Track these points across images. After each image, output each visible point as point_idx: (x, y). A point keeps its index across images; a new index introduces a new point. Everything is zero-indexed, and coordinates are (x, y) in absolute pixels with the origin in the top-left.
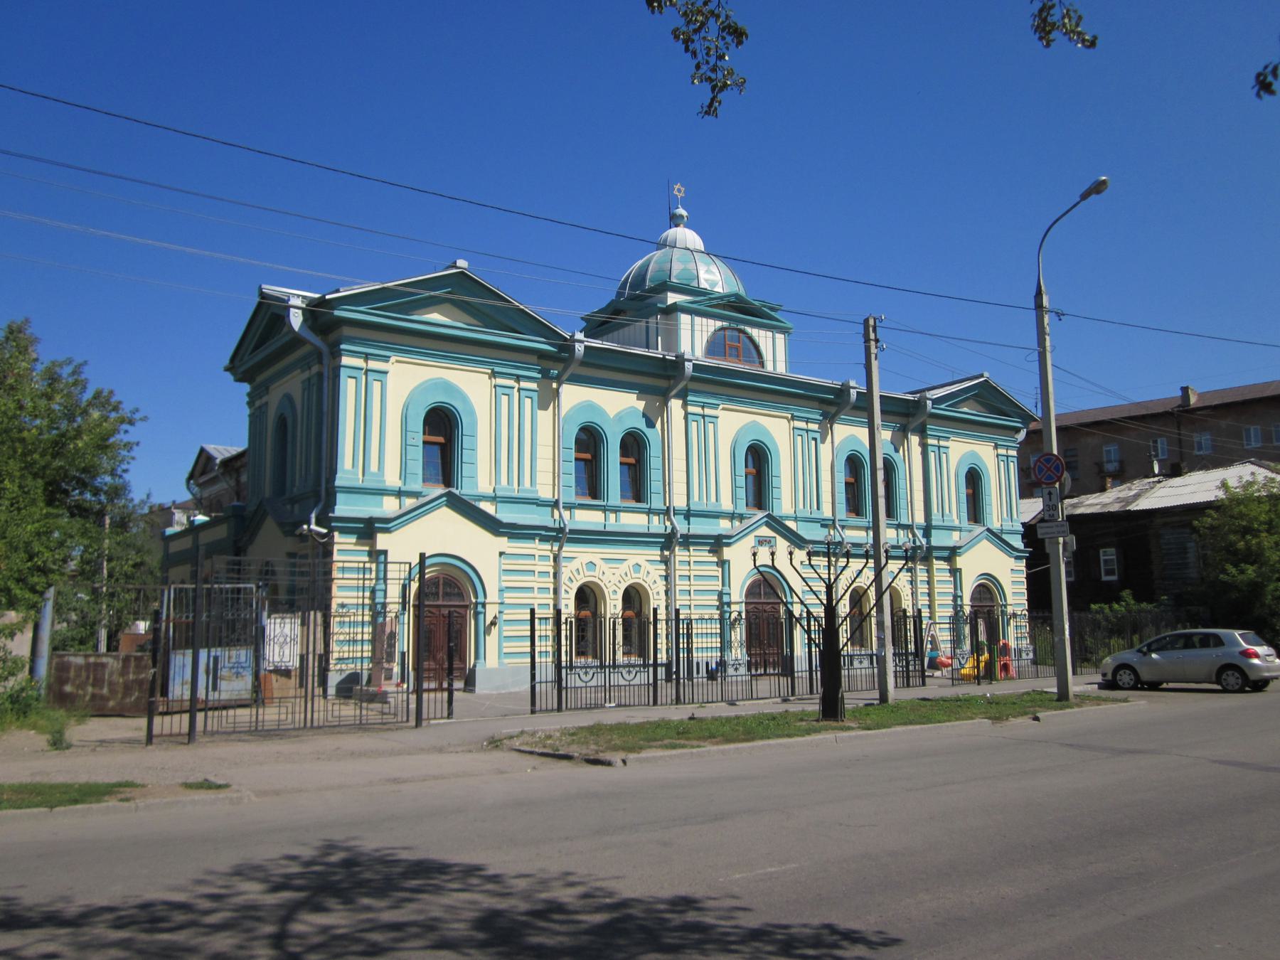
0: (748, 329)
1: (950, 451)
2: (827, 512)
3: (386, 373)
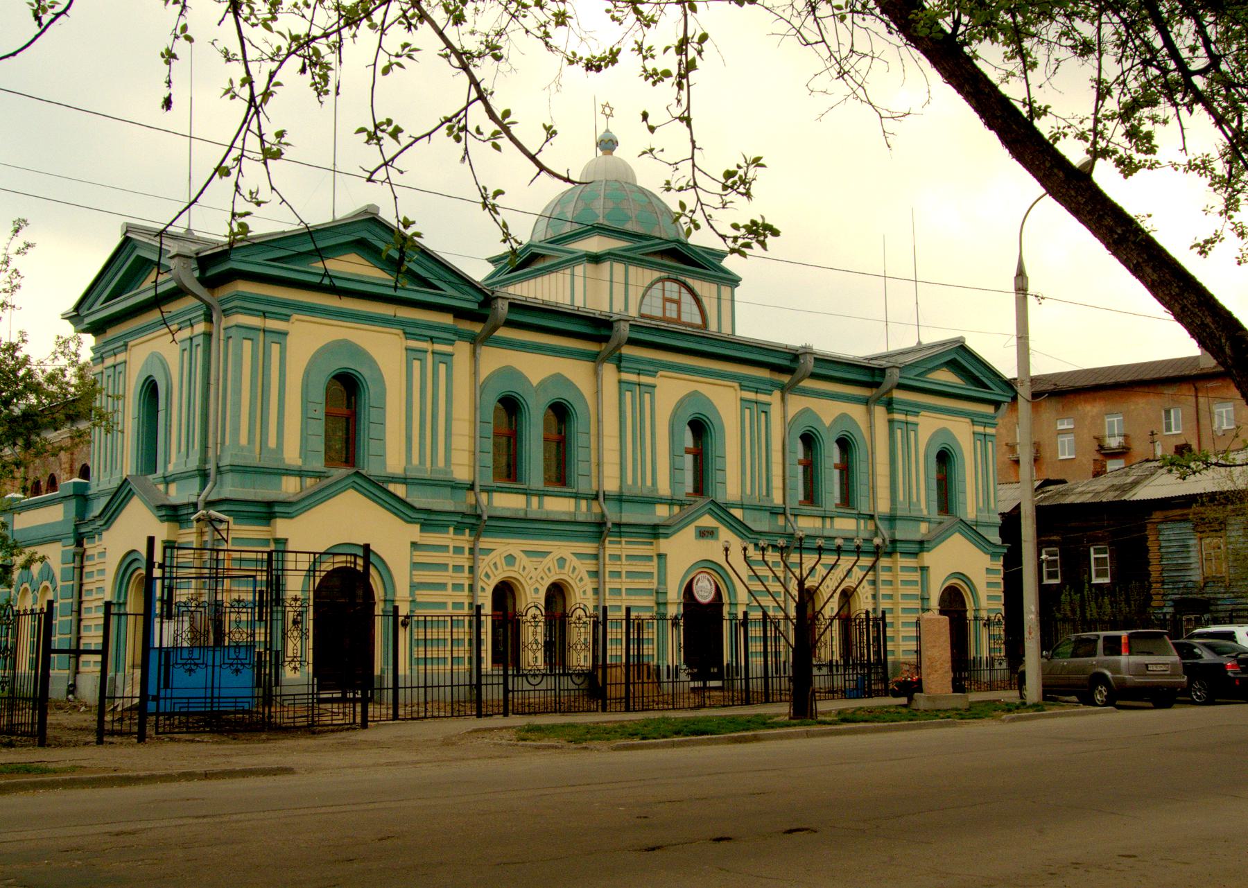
0: (690, 281)
1: (920, 430)
2: (777, 499)
3: (654, 387)
